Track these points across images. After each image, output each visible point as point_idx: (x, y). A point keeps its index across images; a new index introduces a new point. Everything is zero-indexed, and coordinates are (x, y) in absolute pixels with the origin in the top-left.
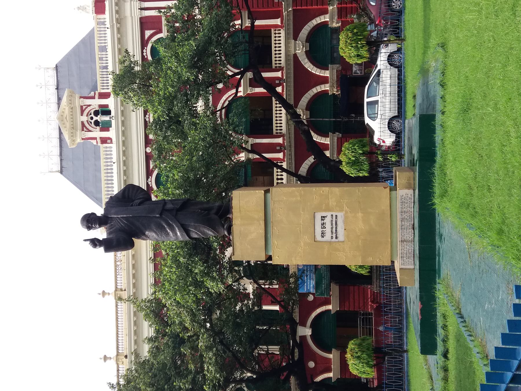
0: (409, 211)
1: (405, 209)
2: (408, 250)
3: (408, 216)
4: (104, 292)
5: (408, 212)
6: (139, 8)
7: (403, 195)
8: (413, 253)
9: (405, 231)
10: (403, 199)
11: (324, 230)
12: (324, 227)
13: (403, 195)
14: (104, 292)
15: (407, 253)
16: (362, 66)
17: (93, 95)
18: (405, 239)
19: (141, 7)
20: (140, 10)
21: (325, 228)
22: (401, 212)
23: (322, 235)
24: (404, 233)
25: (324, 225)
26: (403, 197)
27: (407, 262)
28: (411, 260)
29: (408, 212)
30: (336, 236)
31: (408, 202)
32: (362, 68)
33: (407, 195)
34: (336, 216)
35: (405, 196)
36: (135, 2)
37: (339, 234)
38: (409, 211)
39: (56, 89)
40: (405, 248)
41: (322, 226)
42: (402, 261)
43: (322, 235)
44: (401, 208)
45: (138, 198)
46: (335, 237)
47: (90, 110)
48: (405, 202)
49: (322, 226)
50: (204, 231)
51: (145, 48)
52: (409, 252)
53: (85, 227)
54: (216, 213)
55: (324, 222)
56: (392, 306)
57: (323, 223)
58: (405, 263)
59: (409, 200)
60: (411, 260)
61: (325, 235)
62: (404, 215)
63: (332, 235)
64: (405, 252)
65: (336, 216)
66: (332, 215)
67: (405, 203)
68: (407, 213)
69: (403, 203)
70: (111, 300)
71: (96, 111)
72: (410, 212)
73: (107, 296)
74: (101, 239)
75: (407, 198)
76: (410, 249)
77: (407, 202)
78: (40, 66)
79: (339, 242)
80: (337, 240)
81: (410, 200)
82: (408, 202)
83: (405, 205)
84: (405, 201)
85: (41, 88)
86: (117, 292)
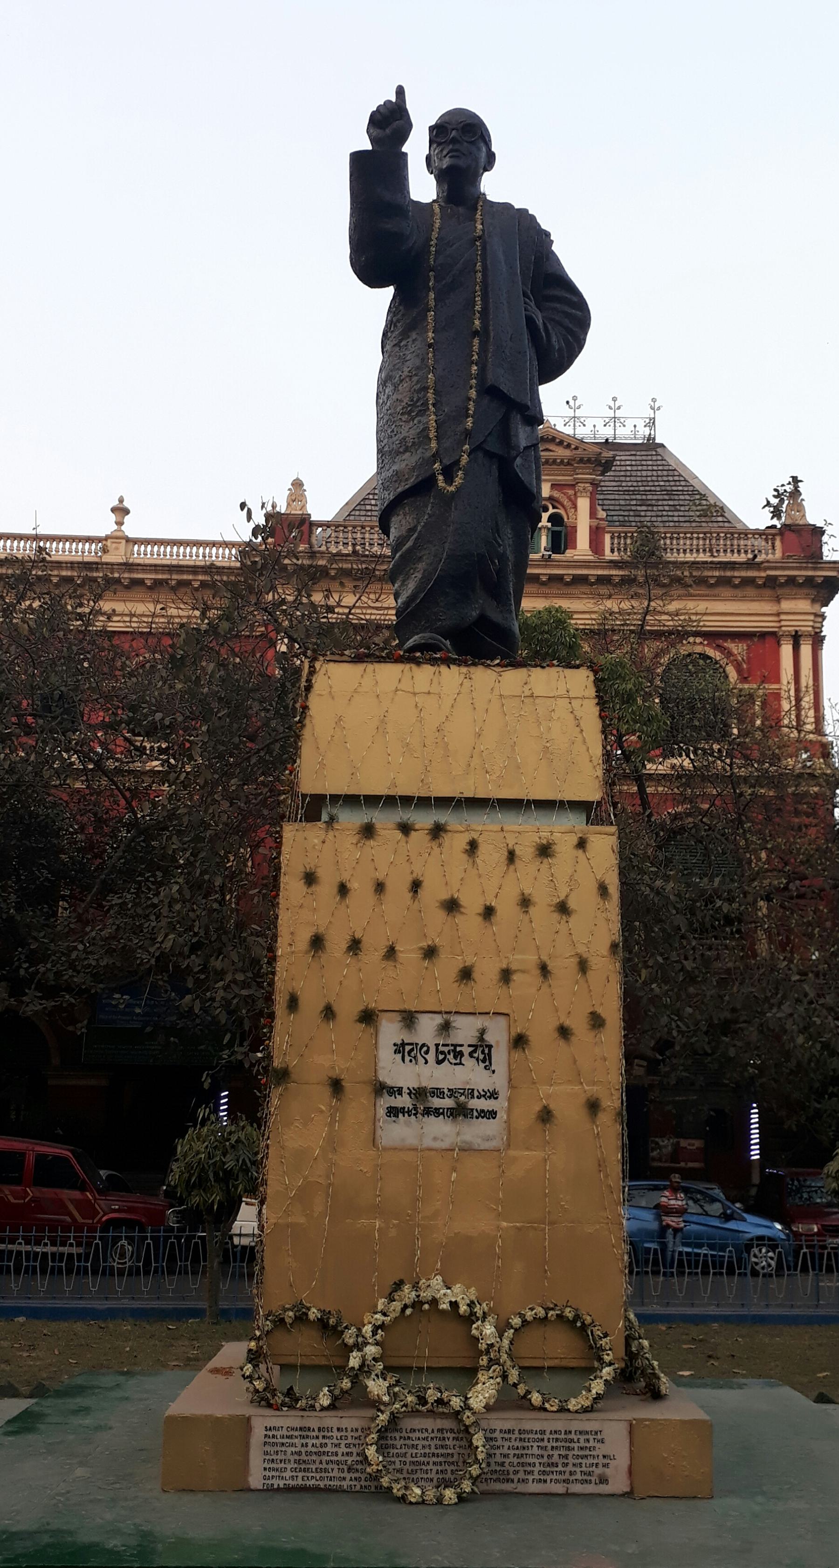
0: (529, 1469)
1: (536, 1451)
2: (338, 1463)
3: (503, 1464)
4: (126, 512)
5: (523, 1465)
6: (800, 633)
7: (602, 1441)
8: (322, 1484)
9: (433, 1450)
10: (582, 1444)
11: (431, 1057)
12: (441, 1057)
13: (602, 1441)
14: (126, 512)
15: (325, 1458)
16: (671, 1162)
17: (599, 517)
18: (394, 1447)
19: (801, 636)
20: (793, 633)
21: (439, 1062)
22: (520, 1432)
23: (408, 1048)
24: (421, 1443)
25: (451, 1057)
26: (592, 1444)
27: (280, 1457)
28: (288, 1474)
29: (523, 1465)
30: (402, 1110)
31: (570, 1468)
32: (666, 1162)
33: (601, 1461)
34: (492, 1114)
35: (601, 1450)
36: (811, 623)
37: (408, 1124)
38: (529, 1469)
39: (607, 440)
40: (348, 1446)
41: (446, 1049)
42: (285, 1433)
43: (408, 1048)
44: (543, 1432)
45: (550, 327)
46: (400, 1105)
47: (563, 506)
48: (571, 1453)
49: (446, 1049)
50: (420, 559)
51: (706, 642)
52: (330, 1466)
53: (447, 118)
54: (483, 619)
55: (466, 1060)
56: (57, 1264)
57: (461, 1054)
58: (274, 1444)
59: (578, 1470)
60: (288, 1474)
61: (407, 1058)
62: (507, 1444)
63: (405, 1090)
64: (329, 1449)
65: (492, 1114)
66: (493, 1095)
67: (563, 1452)
68: (516, 1461)
69: (566, 1440)
70: (105, 526)
71: (562, 518)
72: (521, 1475)
73: (113, 517)
74: (404, 149)
75: (591, 1461)
76: (343, 1471)
77: (571, 1461)
78: (659, 408)
79: (375, 1120)
80: (381, 1112)
81: (578, 1476)
82: (570, 1468)
83: (556, 1453)
84: (576, 1452)
85: (610, 408)
86: (124, 541)
